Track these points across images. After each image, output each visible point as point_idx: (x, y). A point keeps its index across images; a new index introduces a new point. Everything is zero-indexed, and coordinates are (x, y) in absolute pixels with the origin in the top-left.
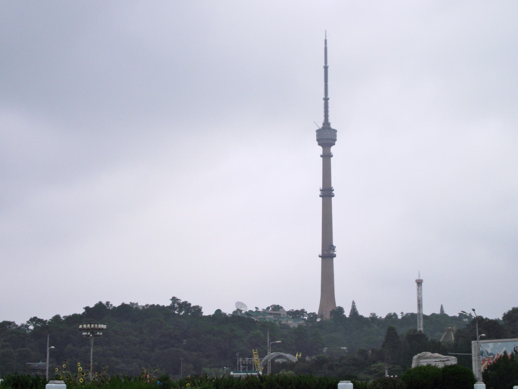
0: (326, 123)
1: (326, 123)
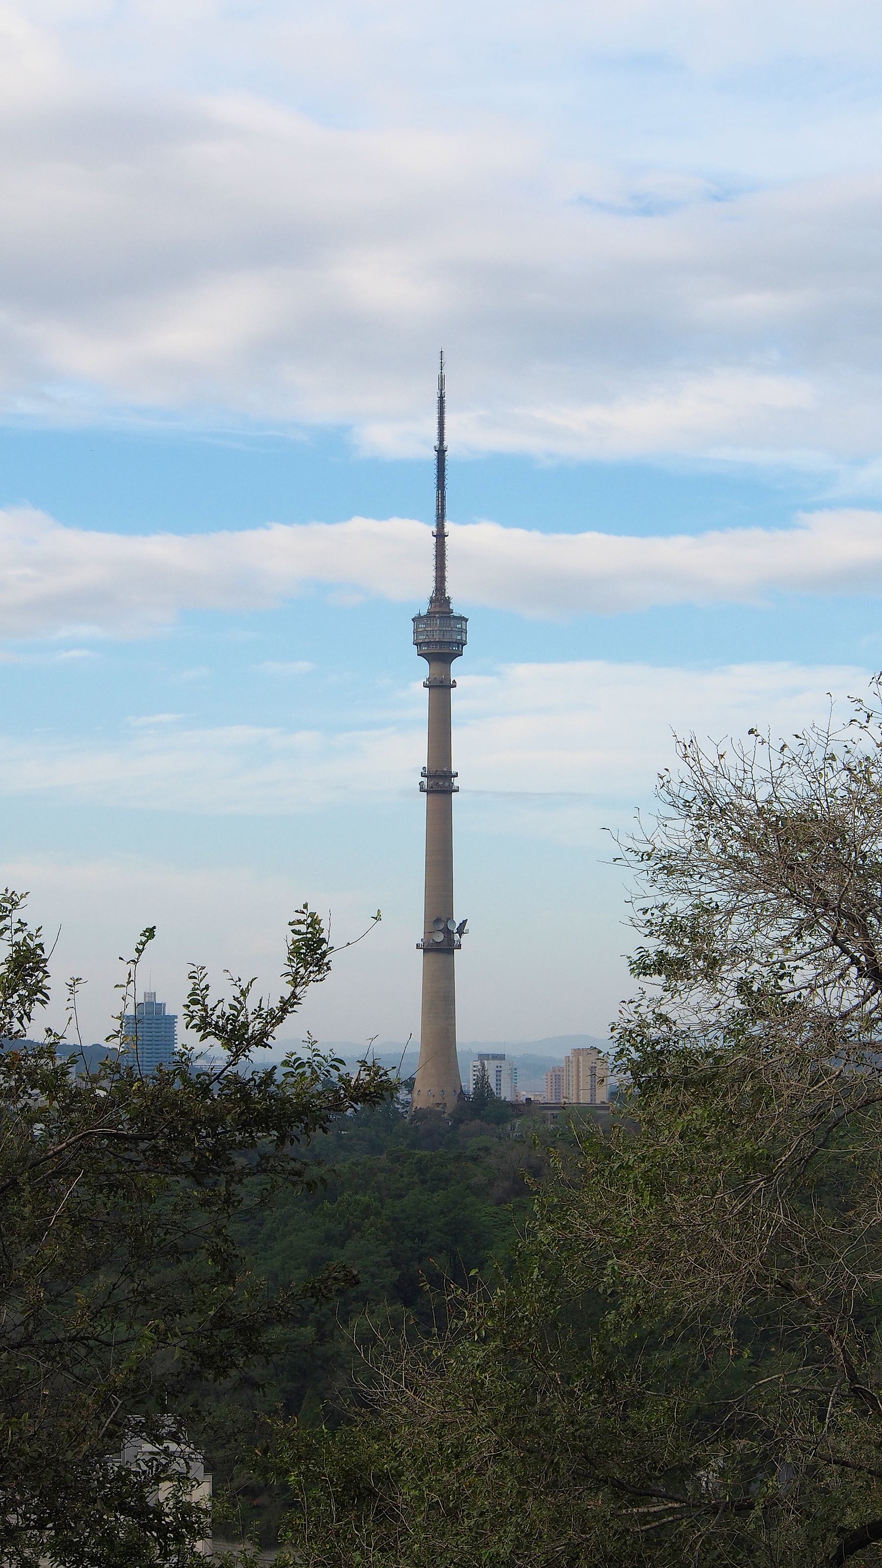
0: (440, 599)
1: (440, 599)
